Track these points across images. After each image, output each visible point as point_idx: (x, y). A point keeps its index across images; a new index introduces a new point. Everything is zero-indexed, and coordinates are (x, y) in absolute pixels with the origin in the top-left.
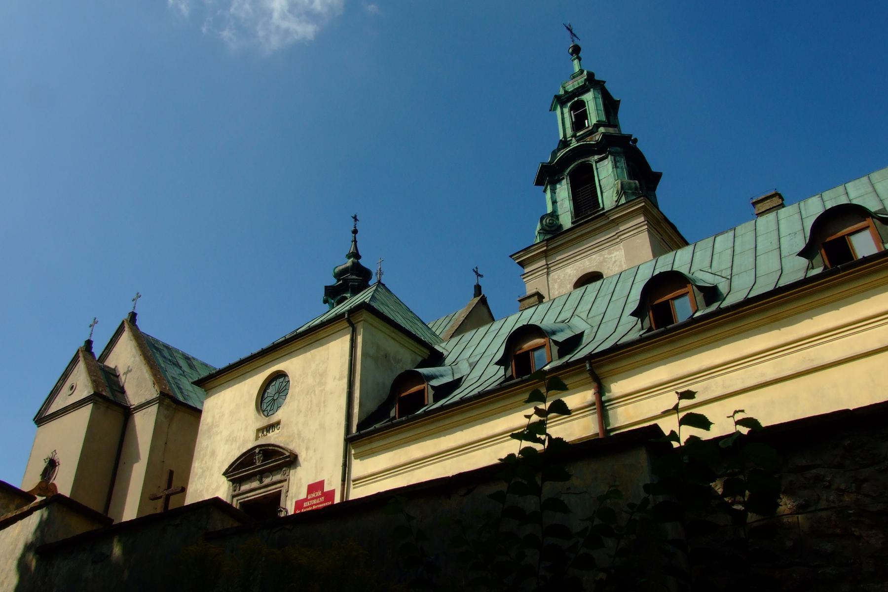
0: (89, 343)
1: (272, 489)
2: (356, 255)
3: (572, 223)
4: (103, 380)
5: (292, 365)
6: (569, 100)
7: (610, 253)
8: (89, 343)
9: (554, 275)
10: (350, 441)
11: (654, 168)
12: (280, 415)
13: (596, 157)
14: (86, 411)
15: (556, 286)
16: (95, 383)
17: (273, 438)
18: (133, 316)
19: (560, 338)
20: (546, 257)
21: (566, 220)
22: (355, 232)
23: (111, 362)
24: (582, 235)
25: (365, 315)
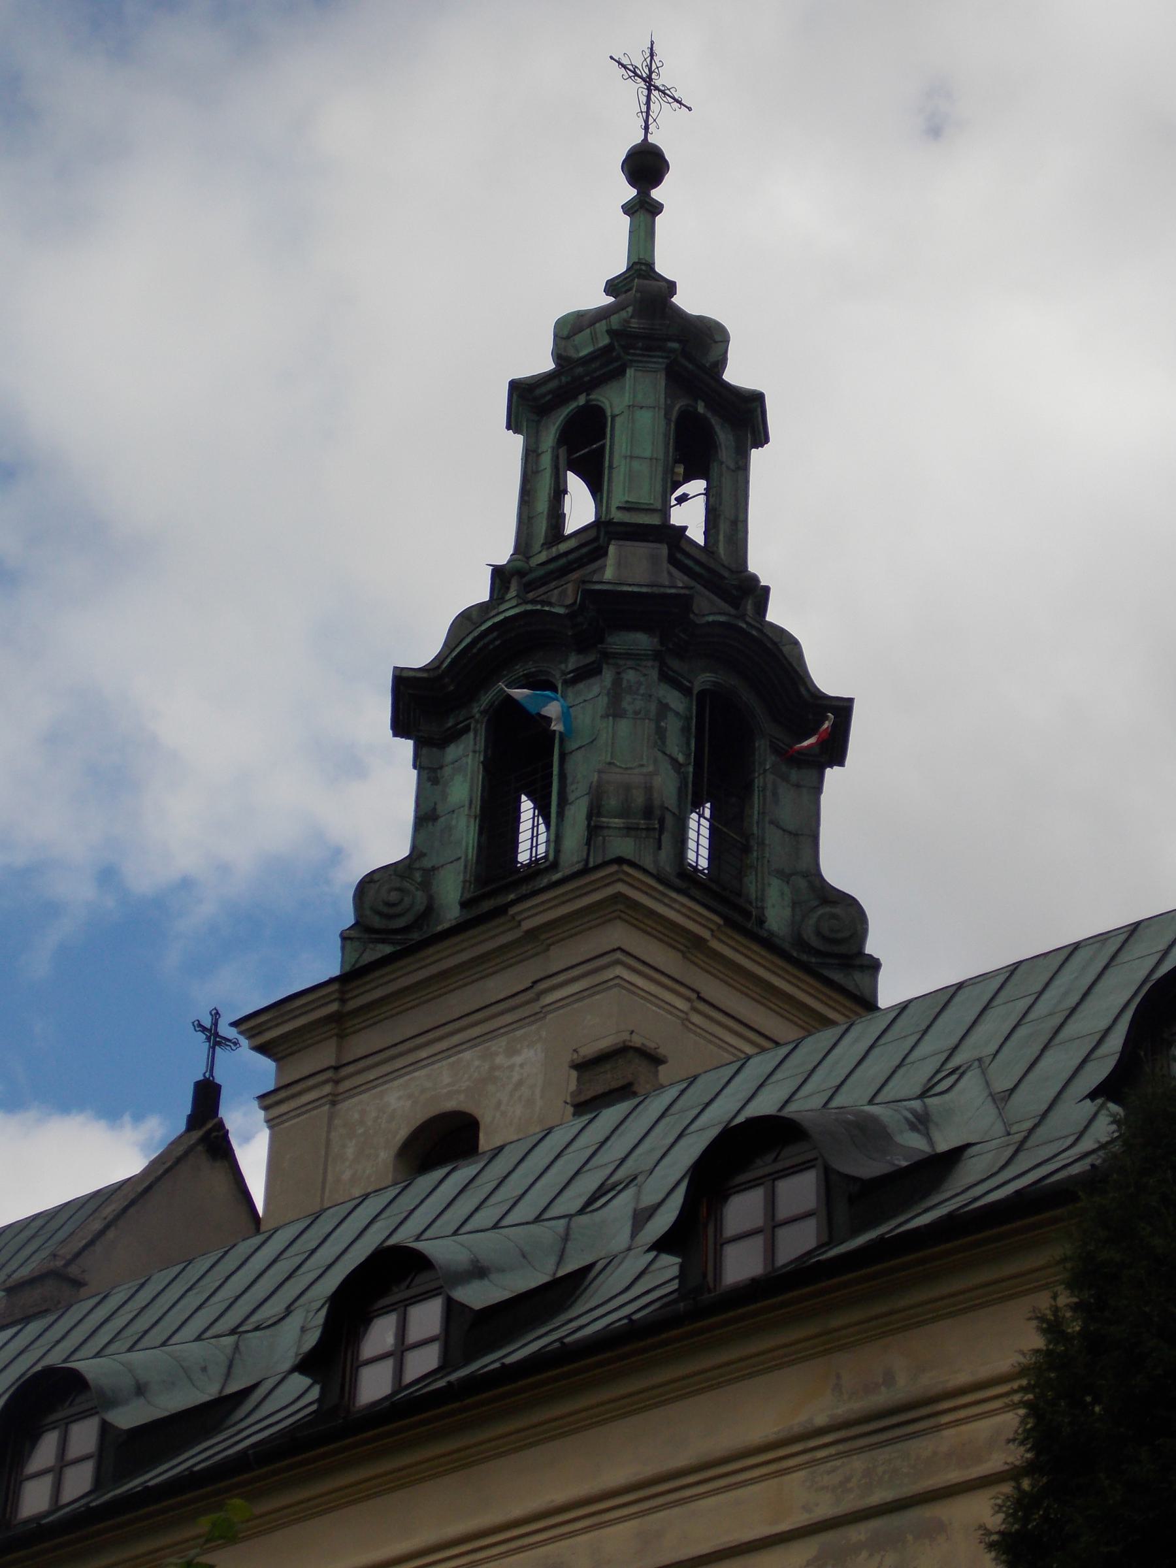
3: (464, 905)
7: (511, 1052)
9: (351, 1108)
11: (827, 674)
13: (573, 662)
15: (350, 1151)
20: (341, 1036)
21: (450, 890)
24: (444, 975)
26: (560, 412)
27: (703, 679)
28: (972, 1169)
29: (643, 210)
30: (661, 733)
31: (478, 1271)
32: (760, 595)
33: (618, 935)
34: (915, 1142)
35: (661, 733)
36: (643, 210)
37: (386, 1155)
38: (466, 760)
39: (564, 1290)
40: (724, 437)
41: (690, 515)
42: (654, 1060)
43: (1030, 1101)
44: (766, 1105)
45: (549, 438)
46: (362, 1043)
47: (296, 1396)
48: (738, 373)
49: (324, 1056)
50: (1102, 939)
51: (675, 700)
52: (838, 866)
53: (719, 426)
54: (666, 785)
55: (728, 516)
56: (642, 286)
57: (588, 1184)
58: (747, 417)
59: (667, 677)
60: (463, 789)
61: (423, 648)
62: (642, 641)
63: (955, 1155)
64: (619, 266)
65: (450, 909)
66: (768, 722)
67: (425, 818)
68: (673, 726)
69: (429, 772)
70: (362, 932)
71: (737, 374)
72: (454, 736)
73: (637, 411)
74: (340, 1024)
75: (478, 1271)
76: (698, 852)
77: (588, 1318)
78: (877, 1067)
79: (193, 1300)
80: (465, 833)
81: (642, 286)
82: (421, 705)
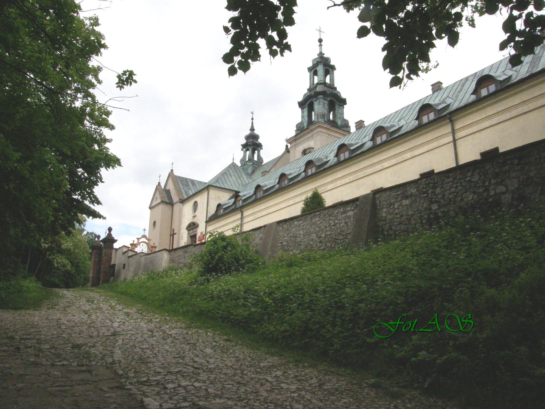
0: (159, 183)
1: (195, 233)
2: (252, 129)
4: (165, 195)
5: (198, 199)
6: (313, 68)
8: (159, 183)
9: (297, 149)
10: (207, 222)
11: (343, 96)
12: (197, 213)
14: (161, 206)
16: (162, 197)
17: (195, 220)
18: (172, 170)
19: (352, 148)
21: (305, 125)
22: (252, 119)
23: (167, 188)
25: (211, 188)
26: (313, 71)
27: (329, 99)
28: (514, 77)
29: (321, 45)
30: (324, 106)
31: (290, 174)
32: (335, 89)
33: (320, 129)
34: (325, 160)
35: (324, 106)
36: (321, 45)
37: (300, 153)
38: (306, 110)
39: (363, 145)
40: (331, 70)
41: (328, 80)
42: (313, 148)
43: (409, 121)
44: (342, 142)
45: (312, 73)
46: (298, 141)
47: (369, 144)
48: (332, 63)
49: (294, 143)
50: (472, 75)
51: (326, 102)
52: (346, 117)
53: (329, 69)
54: (326, 112)
55: (332, 79)
56: (321, 55)
57: (364, 135)
58: (333, 68)
59: (325, 99)
60: (306, 113)
61: (300, 99)
62: (321, 96)
63: (329, 161)
64: (318, 53)
65: (306, 127)
66: (336, 101)
67: (302, 117)
68: (326, 105)
69: (303, 112)
70: (297, 130)
71: (332, 63)
72: (305, 108)
73: (320, 69)
74: (295, 140)
75: (290, 174)
76: (331, 117)
77: (402, 132)
78: (347, 140)
79: (411, 112)
80: (306, 119)
81: (321, 55)
82: (301, 105)
